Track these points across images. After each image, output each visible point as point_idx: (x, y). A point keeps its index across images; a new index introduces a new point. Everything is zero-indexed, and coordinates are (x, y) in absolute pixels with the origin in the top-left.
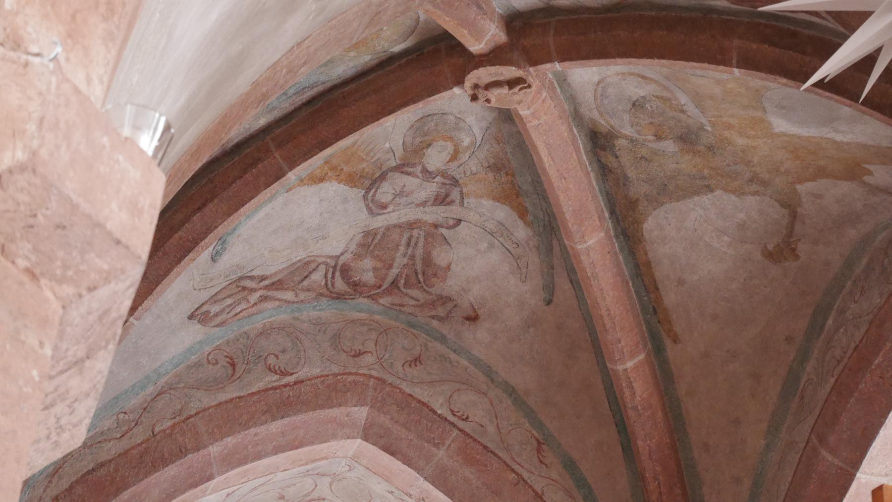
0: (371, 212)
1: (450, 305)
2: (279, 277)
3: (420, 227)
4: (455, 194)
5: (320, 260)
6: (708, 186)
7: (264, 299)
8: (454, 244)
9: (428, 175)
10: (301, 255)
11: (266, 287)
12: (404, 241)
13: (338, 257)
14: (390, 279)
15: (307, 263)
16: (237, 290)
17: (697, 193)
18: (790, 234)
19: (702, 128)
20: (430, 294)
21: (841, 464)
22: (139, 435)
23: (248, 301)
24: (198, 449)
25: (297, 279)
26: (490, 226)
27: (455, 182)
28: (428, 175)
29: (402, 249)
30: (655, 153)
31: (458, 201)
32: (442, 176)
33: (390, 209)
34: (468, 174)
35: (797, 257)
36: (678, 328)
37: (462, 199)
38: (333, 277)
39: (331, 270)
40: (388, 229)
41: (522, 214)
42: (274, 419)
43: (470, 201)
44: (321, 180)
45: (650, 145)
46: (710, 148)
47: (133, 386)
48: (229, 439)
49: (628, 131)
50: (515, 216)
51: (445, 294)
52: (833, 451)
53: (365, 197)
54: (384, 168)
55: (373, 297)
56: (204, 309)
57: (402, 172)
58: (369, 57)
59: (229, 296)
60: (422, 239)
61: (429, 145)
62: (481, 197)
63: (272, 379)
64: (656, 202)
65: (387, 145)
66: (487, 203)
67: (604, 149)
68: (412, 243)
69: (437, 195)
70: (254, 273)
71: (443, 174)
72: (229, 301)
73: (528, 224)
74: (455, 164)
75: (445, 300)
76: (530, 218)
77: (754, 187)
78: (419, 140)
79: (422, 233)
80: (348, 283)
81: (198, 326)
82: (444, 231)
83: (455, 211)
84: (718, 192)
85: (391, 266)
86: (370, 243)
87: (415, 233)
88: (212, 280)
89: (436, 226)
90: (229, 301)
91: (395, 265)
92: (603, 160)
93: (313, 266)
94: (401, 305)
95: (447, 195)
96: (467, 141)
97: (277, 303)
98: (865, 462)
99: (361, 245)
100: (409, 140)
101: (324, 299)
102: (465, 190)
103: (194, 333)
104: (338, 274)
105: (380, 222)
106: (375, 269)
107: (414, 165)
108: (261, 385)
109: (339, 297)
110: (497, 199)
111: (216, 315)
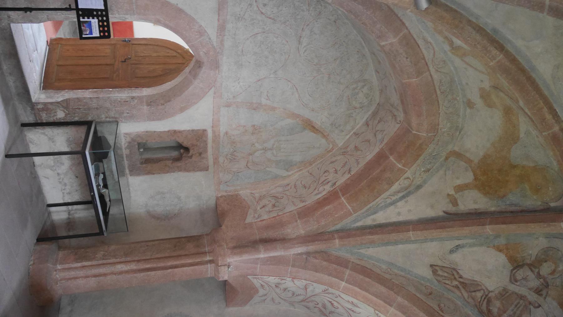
2: (466, 282)
3: (524, 300)
4: (544, 292)
10: (477, 278)
11: (460, 282)
12: (515, 303)
13: (490, 292)
15: (478, 285)
22: (387, 276)
23: (452, 282)
24: (395, 293)
25: (472, 289)
27: (547, 286)
28: (539, 276)
31: (544, 296)
32: (544, 280)
33: (518, 284)
34: (554, 285)
37: (546, 295)
38: (484, 300)
39: (484, 296)
40: (513, 293)
42: (424, 313)
43: (549, 299)
47: (399, 267)
48: (406, 302)
53: (512, 271)
54: (524, 262)
56: (437, 268)
57: (530, 268)
58: (540, 203)
59: (447, 273)
60: (522, 307)
61: (546, 261)
63: (437, 308)
65: (531, 252)
66: (555, 304)
68: (518, 306)
69: (538, 288)
70: (459, 271)
71: (545, 279)
72: (446, 274)
78: (543, 257)
79: (524, 304)
80: (487, 308)
81: (431, 273)
82: (532, 307)
83: (541, 300)
86: (504, 295)
87: (521, 302)
88: (445, 259)
89: (530, 303)
90: (446, 274)
93: (480, 288)
95: (541, 290)
97: (460, 294)
99: (500, 293)
102: (549, 292)
103: (427, 273)
104: (486, 300)
105: (512, 287)
106: (499, 309)
107: (535, 267)
108: (432, 305)
111: (439, 275)
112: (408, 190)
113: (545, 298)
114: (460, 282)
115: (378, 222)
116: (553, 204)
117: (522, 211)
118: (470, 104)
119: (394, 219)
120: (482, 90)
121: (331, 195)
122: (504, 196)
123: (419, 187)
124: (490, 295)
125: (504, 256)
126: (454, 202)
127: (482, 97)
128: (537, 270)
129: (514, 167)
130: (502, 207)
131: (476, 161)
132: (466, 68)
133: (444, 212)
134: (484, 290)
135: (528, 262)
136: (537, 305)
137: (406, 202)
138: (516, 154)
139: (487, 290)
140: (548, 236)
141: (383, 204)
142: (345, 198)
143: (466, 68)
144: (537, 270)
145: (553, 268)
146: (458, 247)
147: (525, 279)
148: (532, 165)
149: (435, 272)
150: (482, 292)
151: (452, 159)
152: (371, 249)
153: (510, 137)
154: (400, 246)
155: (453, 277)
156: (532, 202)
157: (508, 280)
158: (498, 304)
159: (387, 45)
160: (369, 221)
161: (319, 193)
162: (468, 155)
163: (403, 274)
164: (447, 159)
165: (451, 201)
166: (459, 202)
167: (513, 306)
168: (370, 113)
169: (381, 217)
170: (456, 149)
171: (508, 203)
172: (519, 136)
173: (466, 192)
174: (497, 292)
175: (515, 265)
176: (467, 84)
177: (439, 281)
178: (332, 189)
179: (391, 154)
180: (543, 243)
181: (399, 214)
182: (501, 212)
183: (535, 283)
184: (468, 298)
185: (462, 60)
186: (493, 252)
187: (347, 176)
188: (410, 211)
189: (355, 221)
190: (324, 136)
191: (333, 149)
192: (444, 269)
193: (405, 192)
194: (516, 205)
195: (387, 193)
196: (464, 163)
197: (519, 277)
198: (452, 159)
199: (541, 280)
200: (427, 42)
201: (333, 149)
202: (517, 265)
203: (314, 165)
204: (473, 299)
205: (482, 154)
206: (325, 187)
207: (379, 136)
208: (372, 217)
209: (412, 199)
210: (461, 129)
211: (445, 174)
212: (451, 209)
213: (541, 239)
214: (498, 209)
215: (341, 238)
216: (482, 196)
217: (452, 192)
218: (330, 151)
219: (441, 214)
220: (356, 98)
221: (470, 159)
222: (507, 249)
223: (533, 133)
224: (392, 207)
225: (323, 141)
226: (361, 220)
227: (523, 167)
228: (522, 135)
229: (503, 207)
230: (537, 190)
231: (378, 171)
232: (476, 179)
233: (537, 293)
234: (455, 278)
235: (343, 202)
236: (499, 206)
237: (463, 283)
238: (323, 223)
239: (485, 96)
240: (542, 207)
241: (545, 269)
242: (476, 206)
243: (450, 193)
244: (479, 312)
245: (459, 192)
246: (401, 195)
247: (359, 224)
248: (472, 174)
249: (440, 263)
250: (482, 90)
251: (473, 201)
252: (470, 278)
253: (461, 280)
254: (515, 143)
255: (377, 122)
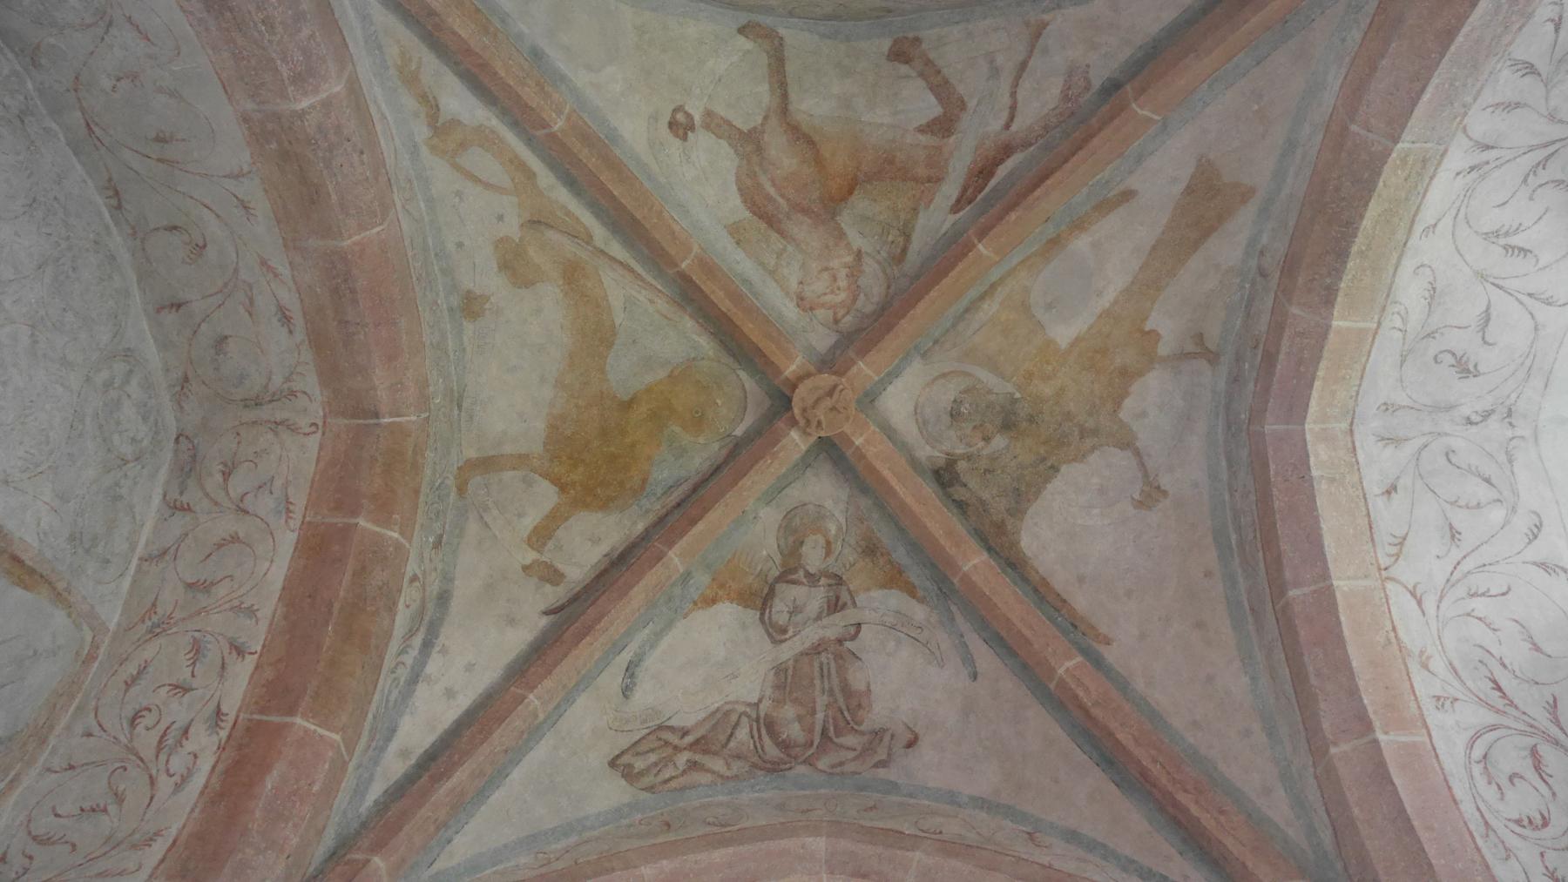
0: (776, 642)
1: (887, 738)
4: (845, 597)
5: (741, 708)
6: (1052, 467)
7: (693, 766)
8: (863, 656)
9: (812, 579)
10: (715, 701)
11: (692, 746)
12: (817, 674)
13: (757, 705)
14: (818, 729)
15: (727, 714)
16: (656, 744)
17: (1047, 480)
18: (1146, 475)
19: (1014, 401)
20: (862, 733)
21: (1313, 588)
25: (723, 738)
26: (890, 620)
28: (812, 579)
29: (817, 682)
30: (993, 458)
33: (790, 633)
35: (1165, 493)
36: (1103, 630)
37: (853, 598)
41: (911, 591)
43: (861, 599)
44: (714, 601)
45: (984, 453)
46: (1031, 419)
48: (665, 862)
49: (960, 450)
50: (905, 597)
51: (877, 727)
52: (1297, 585)
54: (770, 580)
55: (808, 762)
58: (716, 446)
59: (652, 750)
60: (833, 665)
61: (802, 543)
62: (868, 589)
64: (1018, 512)
66: (877, 594)
67: (951, 485)
71: (825, 573)
72: (653, 758)
73: (922, 601)
74: (831, 560)
75: (878, 734)
76: (920, 593)
77: (1089, 442)
78: (791, 539)
80: (777, 744)
82: (848, 644)
83: (851, 615)
84: (1064, 468)
85: (813, 712)
86: (786, 680)
88: (627, 721)
89: (840, 641)
90: (653, 758)
91: (818, 708)
92: (956, 497)
93: (734, 718)
94: (841, 764)
95: (838, 598)
96: (833, 529)
98: (1331, 566)
99: (777, 687)
100: (782, 542)
101: (760, 773)
103: (613, 793)
104: (764, 732)
105: (788, 651)
106: (800, 718)
107: (795, 570)
109: (774, 768)
110: (883, 586)
111: (641, 774)
112: (427, 619)
113: (854, 603)
114: (692, 746)
115: (421, 751)
116: (739, 432)
117: (695, 489)
118: (471, 306)
119: (450, 714)
120: (500, 243)
121: (240, 747)
122: (644, 481)
123: (444, 599)
124: (762, 714)
125: (728, 604)
126: (552, 575)
127: (505, 266)
128: (801, 573)
129: (628, 405)
130: (655, 507)
131: (537, 448)
132: (459, 194)
133: (546, 613)
134: (744, 713)
135: (775, 573)
136: (852, 630)
137: (444, 651)
138: (623, 373)
139: (749, 705)
140: (770, 497)
141: (395, 693)
142: (304, 716)
143: (459, 194)
144: (801, 573)
145: (822, 541)
146: (631, 670)
147: (795, 610)
148: (662, 374)
149: (629, 775)
150: (744, 720)
151: (476, 480)
152: (457, 840)
153: (596, 337)
154: (516, 775)
155: (669, 750)
156: (701, 453)
157: (767, 644)
158: (789, 711)
159: (312, 107)
160: (393, 767)
161: (185, 779)
162: (508, 449)
163: (573, 839)
164: (461, 490)
165: (542, 579)
166: (560, 566)
167: (817, 682)
168: (163, 474)
169: (418, 729)
170: (471, 453)
171: (659, 491)
172: (613, 326)
173: (560, 533)
174: (769, 692)
175: (759, 602)
176: (460, 245)
177: (650, 789)
178: (224, 734)
179: (354, 513)
180: (770, 517)
181: (450, 693)
182: (661, 521)
183: (815, 599)
184: (728, 765)
185: (457, 167)
186: (701, 617)
187: (242, 671)
188: (470, 667)
189: (359, 792)
190: (60, 598)
191: (95, 646)
192: (641, 748)
193: (423, 629)
194: (677, 484)
195: (394, 646)
196: (511, 473)
197: (781, 618)
198: (476, 480)
199: (823, 581)
200: (384, 117)
201: (95, 646)
202: (760, 599)
203: (52, 741)
204: (738, 757)
205: (540, 426)
206: (189, 746)
207: (265, 505)
208: (394, 746)
209: (450, 635)
210: (461, 397)
211: (487, 525)
212: (554, 595)
213: (762, 514)
214: (652, 518)
215: (378, 846)
216: (600, 515)
217: (531, 556)
218: (91, 658)
219: (544, 621)
220: (118, 423)
221: (520, 456)
222: (722, 586)
223: (641, 298)
224: (422, 690)
225: (60, 618)
226: (371, 779)
227: (649, 390)
228: (619, 318)
229: (657, 508)
230: (698, 422)
231: (347, 578)
232: (563, 488)
233: (835, 611)
234: (675, 748)
235: (306, 731)
236: (647, 511)
237: (697, 742)
238: (295, 841)
239: (513, 263)
240: (724, 452)
241: (813, 557)
242: (604, 548)
243: (528, 561)
244: (769, 771)
245: (545, 544)
246: (417, 641)
247: (375, 792)
248: (546, 484)
249: (624, 742)
250: (500, 243)
251: (588, 542)
252: (703, 715)
253: (689, 739)
254: (610, 345)
255: (219, 478)
